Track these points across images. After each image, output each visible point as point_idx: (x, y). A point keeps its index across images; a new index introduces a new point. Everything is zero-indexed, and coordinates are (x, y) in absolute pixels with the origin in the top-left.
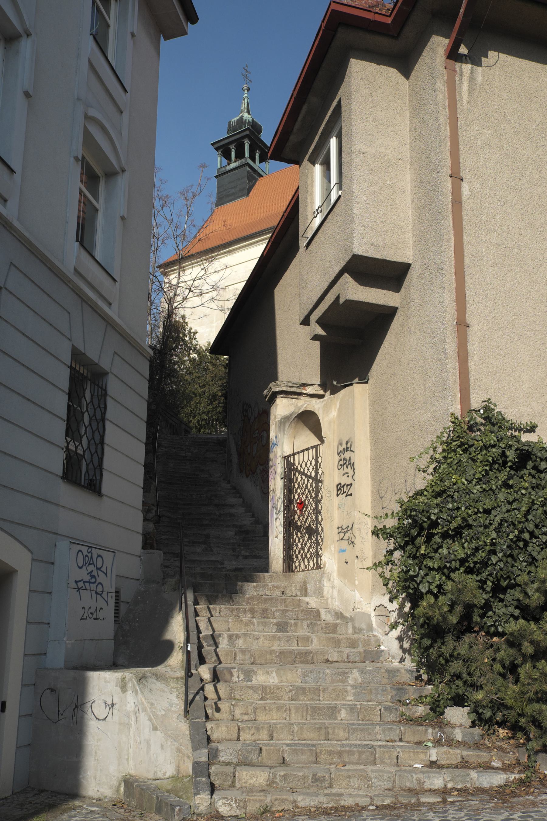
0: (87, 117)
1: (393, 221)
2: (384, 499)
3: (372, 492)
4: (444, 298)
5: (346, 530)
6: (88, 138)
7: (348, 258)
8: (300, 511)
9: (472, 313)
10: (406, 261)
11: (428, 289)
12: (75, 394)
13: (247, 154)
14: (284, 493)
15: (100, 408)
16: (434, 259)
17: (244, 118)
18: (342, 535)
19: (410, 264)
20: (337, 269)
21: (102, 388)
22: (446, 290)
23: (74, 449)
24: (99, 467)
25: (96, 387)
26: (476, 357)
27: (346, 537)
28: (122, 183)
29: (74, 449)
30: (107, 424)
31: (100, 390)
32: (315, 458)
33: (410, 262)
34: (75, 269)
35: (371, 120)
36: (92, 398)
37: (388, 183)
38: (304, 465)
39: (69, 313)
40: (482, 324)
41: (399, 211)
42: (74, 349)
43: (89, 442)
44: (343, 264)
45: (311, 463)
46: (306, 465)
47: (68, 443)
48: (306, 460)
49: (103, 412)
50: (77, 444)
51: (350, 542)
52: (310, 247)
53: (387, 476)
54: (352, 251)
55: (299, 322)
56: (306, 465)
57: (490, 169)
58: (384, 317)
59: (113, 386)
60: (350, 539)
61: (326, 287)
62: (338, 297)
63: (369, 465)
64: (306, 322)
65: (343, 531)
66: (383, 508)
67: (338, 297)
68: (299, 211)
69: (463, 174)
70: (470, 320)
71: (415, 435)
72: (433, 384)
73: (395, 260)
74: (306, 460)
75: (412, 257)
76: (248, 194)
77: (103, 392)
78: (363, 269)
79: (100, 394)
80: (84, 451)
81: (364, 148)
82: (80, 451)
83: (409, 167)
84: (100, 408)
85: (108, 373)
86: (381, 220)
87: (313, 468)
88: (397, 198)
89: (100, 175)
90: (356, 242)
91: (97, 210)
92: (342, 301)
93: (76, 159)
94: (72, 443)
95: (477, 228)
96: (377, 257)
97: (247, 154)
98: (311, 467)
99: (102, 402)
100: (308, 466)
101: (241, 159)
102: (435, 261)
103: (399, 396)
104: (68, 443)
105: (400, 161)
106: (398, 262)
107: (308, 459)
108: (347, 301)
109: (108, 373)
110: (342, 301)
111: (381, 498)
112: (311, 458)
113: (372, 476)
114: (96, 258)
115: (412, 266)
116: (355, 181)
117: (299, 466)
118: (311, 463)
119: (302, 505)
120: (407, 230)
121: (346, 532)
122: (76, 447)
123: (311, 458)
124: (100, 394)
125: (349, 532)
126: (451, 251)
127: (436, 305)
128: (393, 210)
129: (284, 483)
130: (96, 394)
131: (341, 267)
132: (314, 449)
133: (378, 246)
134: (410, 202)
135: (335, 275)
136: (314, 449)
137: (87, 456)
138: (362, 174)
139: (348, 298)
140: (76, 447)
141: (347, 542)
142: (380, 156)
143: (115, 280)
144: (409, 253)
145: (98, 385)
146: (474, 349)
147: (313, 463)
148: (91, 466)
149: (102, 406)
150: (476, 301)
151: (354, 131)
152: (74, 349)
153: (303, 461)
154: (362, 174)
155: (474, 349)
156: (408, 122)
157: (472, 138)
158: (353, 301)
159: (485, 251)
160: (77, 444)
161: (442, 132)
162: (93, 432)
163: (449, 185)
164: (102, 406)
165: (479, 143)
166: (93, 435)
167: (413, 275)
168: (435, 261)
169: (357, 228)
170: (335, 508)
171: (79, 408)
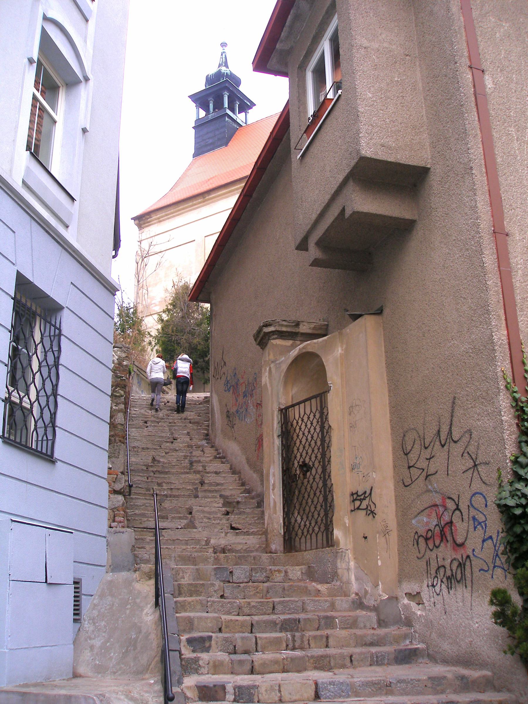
0: (46, 18)
1: (405, 121)
2: (411, 455)
3: (394, 448)
4: (476, 201)
5: (362, 497)
6: (45, 37)
7: (353, 163)
8: (304, 475)
9: (511, 219)
10: (423, 165)
11: (453, 194)
12: (20, 333)
13: (226, 105)
14: (282, 454)
15: (52, 351)
16: (459, 158)
17: (223, 71)
18: (357, 503)
19: (429, 169)
20: (341, 178)
21: (55, 326)
22: (479, 193)
23: (18, 401)
24: (51, 425)
25: (48, 325)
26: (520, 272)
27: (364, 506)
28: (84, 94)
29: (18, 401)
30: (61, 369)
31: (53, 328)
32: (319, 408)
33: (429, 166)
34: (24, 182)
35: (371, 15)
36: (42, 338)
37: (396, 79)
38: (305, 419)
39: (14, 232)
40: (523, 232)
41: (411, 109)
42: (19, 276)
43: (38, 392)
44: (347, 171)
45: (314, 416)
46: (309, 418)
47: (10, 394)
48: (308, 412)
49: (56, 355)
50: (22, 394)
51: (369, 512)
52: (307, 159)
53: (413, 427)
54: (358, 152)
55: (293, 247)
56: (309, 418)
57: (513, 62)
58: (399, 231)
59: (68, 323)
60: (369, 508)
61: (327, 201)
62: (343, 210)
63: (388, 415)
64: (303, 246)
65: (358, 498)
66: (409, 467)
67: (343, 210)
68: (290, 126)
69: (485, 65)
70: (508, 226)
71: (448, 372)
72: (470, 307)
73: (410, 163)
74: (308, 412)
75: (430, 161)
76: (226, 144)
77: (57, 331)
78: (372, 174)
79: (52, 333)
80: (32, 405)
81: (366, 43)
82: (26, 404)
83: (418, 64)
84: (52, 351)
85: (64, 308)
86: (391, 119)
87: (318, 422)
88: (407, 95)
89: (59, 84)
90: (363, 142)
91: (55, 122)
92: (347, 215)
93: (31, 61)
94: (15, 394)
95: (506, 124)
96: (389, 160)
97: (226, 105)
98: (315, 420)
99: (55, 343)
100: (311, 419)
101: (219, 109)
102: (461, 160)
103: (423, 326)
104: (10, 394)
105: (408, 57)
106: (414, 166)
107: (311, 411)
108: (354, 213)
109: (64, 308)
110: (347, 215)
111: (406, 454)
112: (314, 410)
113: (392, 428)
114: (52, 172)
115: (432, 170)
116: (358, 77)
117: (300, 419)
118: (314, 416)
119: (305, 467)
120: (421, 130)
121: (361, 500)
122: (21, 399)
123: (314, 410)
124: (52, 333)
125: (368, 499)
126: (479, 148)
127: (466, 211)
128: (405, 108)
129: (282, 441)
130: (47, 334)
131: (345, 174)
132: (318, 399)
133: (390, 148)
134: (423, 100)
135: (338, 185)
136: (318, 399)
137: (36, 411)
138: (366, 69)
139: (356, 209)
140: (21, 399)
141: (365, 512)
142: (384, 51)
143: (73, 199)
144: (426, 156)
145: (50, 323)
146: (517, 262)
147: (318, 415)
148: (40, 424)
149: (55, 348)
150: (514, 205)
151: (353, 24)
152: (19, 276)
153: (305, 413)
154: (366, 69)
155: (517, 262)
156: (414, 18)
157: (490, 29)
158: (362, 212)
159: (518, 149)
160: (22, 394)
161: (456, 21)
162: (44, 381)
163: (470, 76)
164: (55, 348)
165: (498, 35)
166: (44, 384)
167: (434, 180)
168: (461, 160)
169: (364, 128)
170: (348, 470)
171: (24, 350)
